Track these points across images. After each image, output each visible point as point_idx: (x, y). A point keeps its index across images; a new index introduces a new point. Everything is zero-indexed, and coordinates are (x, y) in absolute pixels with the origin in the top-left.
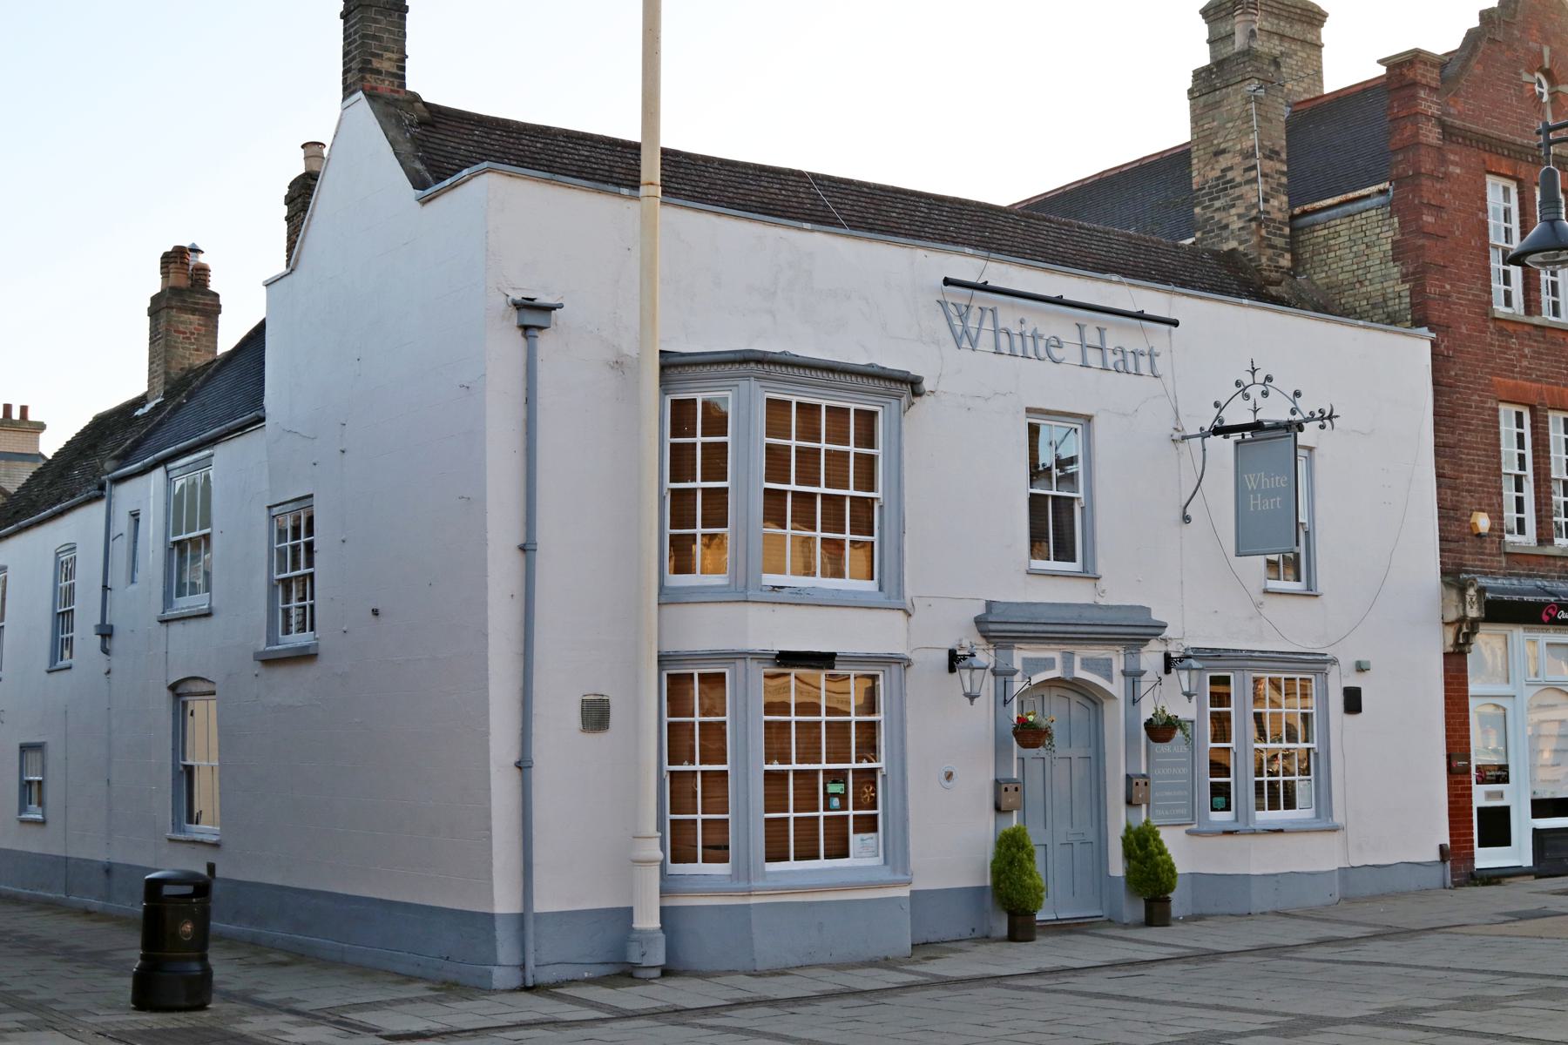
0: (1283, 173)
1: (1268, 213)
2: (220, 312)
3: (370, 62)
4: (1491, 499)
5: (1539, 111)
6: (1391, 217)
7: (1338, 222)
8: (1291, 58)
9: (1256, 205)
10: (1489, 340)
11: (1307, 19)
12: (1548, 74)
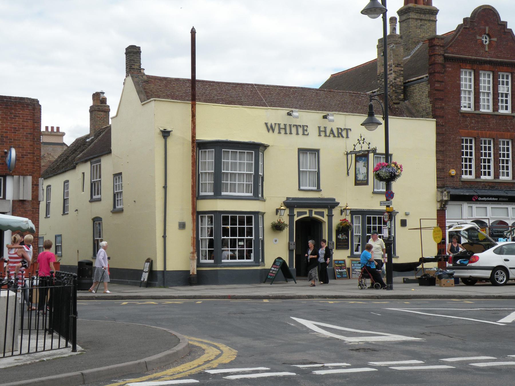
0: (402, 71)
1: (396, 83)
2: (110, 111)
3: (132, 66)
4: (457, 165)
5: (483, 47)
6: (428, 84)
7: (416, 85)
8: (424, 26)
9: (392, 81)
10: (459, 119)
11: (431, 13)
12: (488, 35)
